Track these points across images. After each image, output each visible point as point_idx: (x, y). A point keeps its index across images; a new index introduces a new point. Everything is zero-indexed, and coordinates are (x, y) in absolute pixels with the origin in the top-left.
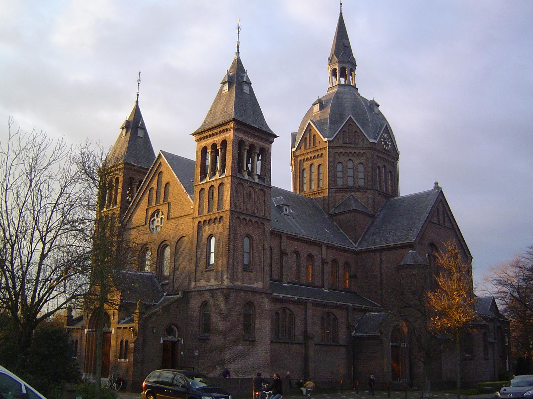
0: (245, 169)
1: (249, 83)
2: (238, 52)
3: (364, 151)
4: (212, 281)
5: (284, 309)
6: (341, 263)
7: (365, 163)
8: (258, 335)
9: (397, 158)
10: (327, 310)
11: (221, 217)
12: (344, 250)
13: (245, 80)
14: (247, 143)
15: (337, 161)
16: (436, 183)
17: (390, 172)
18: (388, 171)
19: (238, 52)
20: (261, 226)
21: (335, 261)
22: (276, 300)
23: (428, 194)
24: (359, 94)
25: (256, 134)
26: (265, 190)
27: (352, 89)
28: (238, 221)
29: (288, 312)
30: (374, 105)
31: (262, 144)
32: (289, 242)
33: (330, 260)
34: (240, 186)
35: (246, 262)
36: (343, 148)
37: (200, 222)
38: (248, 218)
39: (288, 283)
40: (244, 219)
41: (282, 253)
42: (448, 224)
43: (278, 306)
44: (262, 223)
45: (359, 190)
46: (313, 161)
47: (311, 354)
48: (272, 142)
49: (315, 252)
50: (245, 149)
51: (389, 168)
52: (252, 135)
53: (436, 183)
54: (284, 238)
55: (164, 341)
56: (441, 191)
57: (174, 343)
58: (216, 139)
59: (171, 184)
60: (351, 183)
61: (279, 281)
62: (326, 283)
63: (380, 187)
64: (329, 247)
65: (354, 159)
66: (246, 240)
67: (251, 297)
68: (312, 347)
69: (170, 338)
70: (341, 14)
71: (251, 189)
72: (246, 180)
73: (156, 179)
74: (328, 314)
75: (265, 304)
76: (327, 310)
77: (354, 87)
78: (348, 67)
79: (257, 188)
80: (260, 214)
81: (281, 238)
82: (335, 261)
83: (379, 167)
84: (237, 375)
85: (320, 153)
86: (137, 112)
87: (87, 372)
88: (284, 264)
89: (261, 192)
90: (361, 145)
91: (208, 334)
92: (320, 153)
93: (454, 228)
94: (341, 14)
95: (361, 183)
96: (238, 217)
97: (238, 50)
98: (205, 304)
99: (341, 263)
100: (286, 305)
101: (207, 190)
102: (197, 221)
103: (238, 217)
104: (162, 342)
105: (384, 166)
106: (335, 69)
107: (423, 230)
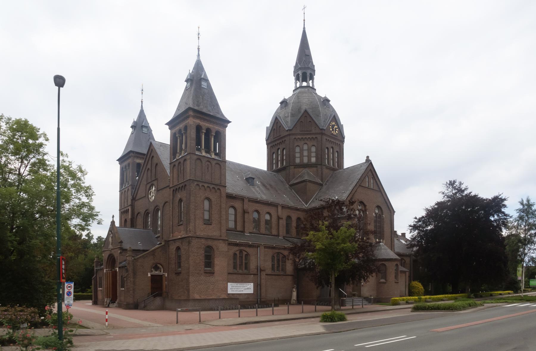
0: (213, 150)
1: (207, 80)
2: (199, 55)
3: (316, 136)
4: (182, 232)
5: (241, 251)
6: (294, 218)
7: (316, 145)
8: (217, 268)
9: (343, 141)
10: (277, 251)
11: (185, 185)
12: (297, 209)
13: (202, 77)
14: (204, 128)
15: (296, 144)
16: (368, 157)
17: (337, 152)
18: (335, 151)
19: (199, 55)
20: (218, 191)
21: (289, 218)
22: (230, 244)
23: (361, 165)
24: (316, 94)
25: (203, 117)
26: (220, 163)
27: (310, 89)
28: (198, 188)
29: (245, 253)
30: (326, 101)
31: (217, 128)
32: (250, 203)
33: (284, 217)
34: (198, 161)
35: (207, 217)
36: (301, 134)
37: (174, 190)
38: (206, 185)
39: (250, 233)
40: (203, 186)
41: (244, 212)
42: (376, 188)
43: (236, 248)
44: (219, 189)
45: (309, 165)
46: (278, 147)
47: (263, 282)
48: (226, 126)
49: (272, 210)
50: (202, 132)
51: (336, 149)
52: (205, 120)
53: (368, 157)
54: (246, 201)
55: (151, 275)
56: (371, 163)
57: (161, 276)
58: (181, 126)
59: (159, 164)
60: (305, 160)
61: (242, 232)
62: (281, 233)
63: (328, 163)
64: (283, 207)
65: (308, 142)
66: (206, 203)
67: (210, 243)
68: (263, 276)
69: (157, 273)
70: (304, 28)
71: (209, 163)
72: (204, 156)
73: (150, 162)
74: (278, 253)
75: (222, 247)
76: (277, 251)
77: (313, 88)
78: (308, 72)
79: (214, 163)
80: (217, 182)
81: (243, 201)
82: (289, 218)
83: (327, 148)
84: (200, 297)
85: (284, 140)
86: (142, 115)
87: (107, 298)
88: (246, 220)
89: (217, 166)
90: (314, 131)
91: (180, 269)
92: (284, 140)
93: (380, 191)
94: (304, 28)
95: (313, 160)
96: (197, 185)
97: (199, 53)
98: (178, 248)
99: (294, 218)
100: (242, 248)
101: (177, 165)
102: (172, 189)
103: (197, 185)
104: (149, 275)
105: (332, 147)
106: (298, 74)
107: (354, 192)
